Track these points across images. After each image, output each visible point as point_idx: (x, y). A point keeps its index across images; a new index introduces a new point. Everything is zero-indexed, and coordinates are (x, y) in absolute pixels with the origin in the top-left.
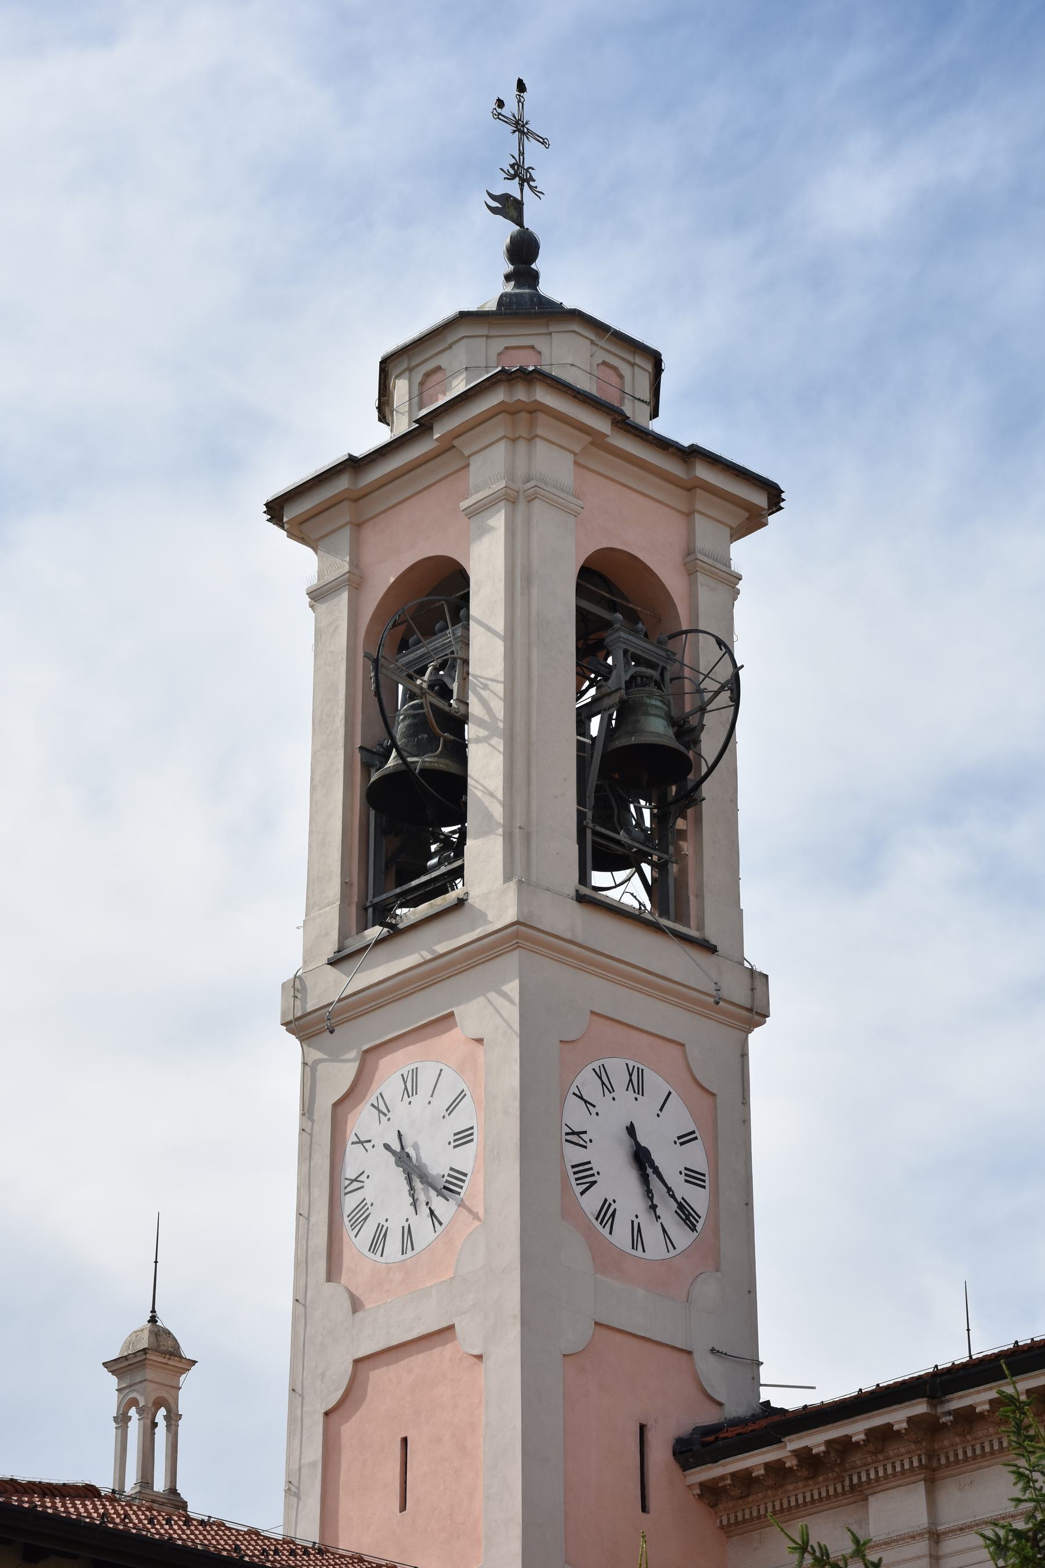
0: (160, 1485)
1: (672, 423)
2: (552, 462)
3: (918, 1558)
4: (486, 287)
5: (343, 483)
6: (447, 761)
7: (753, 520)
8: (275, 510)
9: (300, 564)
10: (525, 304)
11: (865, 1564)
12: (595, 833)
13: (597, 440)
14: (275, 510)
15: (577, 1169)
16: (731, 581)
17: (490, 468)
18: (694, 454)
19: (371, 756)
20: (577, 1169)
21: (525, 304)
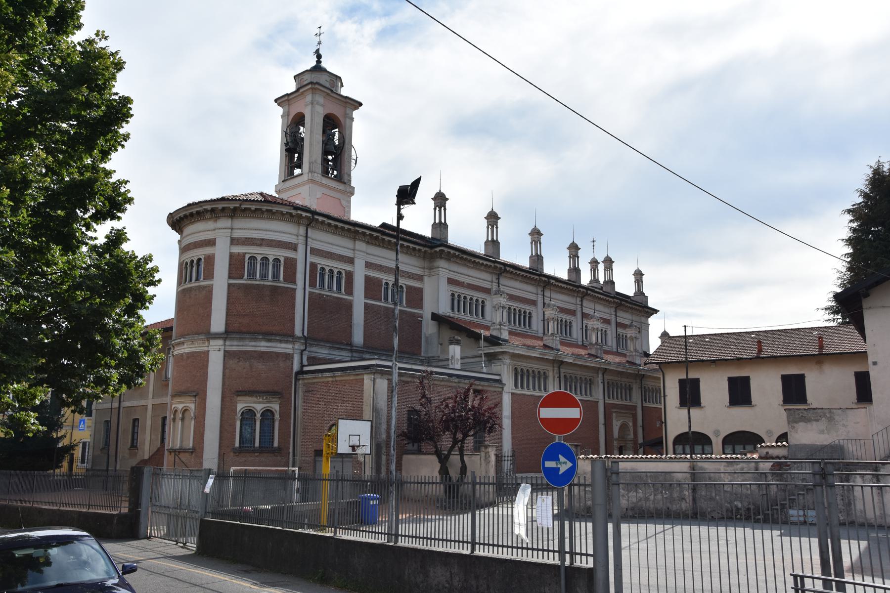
0: (567, 524)
1: (344, 92)
2: (320, 99)
3: (690, 427)
4: (313, 63)
5: (286, 98)
6: (319, 192)
7: (356, 108)
8: (276, 101)
9: (280, 111)
10: (318, 68)
11: (795, 493)
12: (368, 265)
13: (328, 94)
14: (276, 101)
15: (540, 530)
16: (352, 119)
17: (309, 98)
18: (346, 97)
19: (286, 144)
20: (540, 530)
21: (318, 68)
